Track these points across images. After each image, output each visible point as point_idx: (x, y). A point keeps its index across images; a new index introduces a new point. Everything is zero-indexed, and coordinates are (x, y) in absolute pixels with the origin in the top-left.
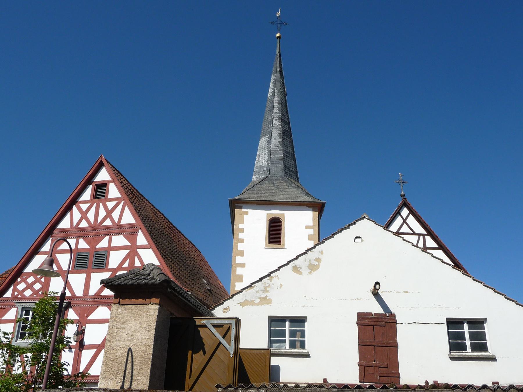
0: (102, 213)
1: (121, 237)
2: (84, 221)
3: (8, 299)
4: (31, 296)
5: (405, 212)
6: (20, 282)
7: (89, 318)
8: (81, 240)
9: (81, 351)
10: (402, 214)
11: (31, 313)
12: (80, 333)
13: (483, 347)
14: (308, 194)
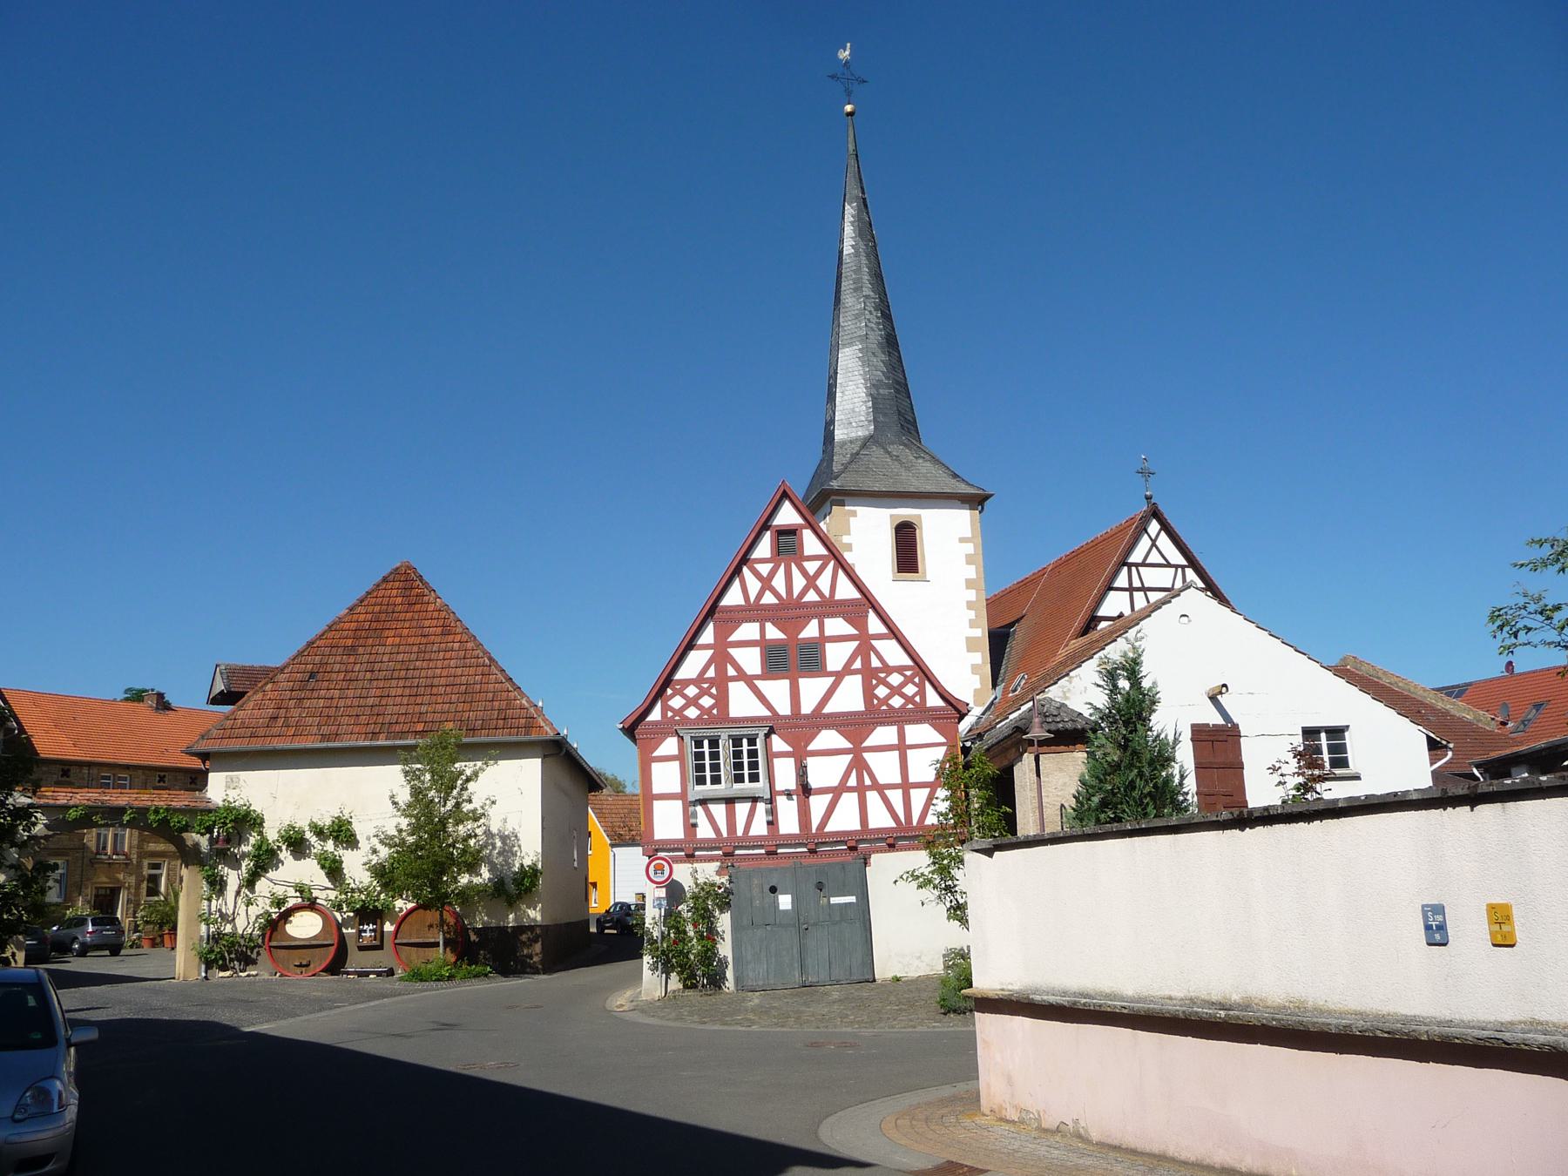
0: (799, 582)
1: (840, 620)
2: (768, 593)
3: (655, 723)
5: (1154, 527)
6: (672, 696)
8: (769, 626)
11: (706, 743)
12: (802, 772)
13: (1343, 763)
14: (955, 476)
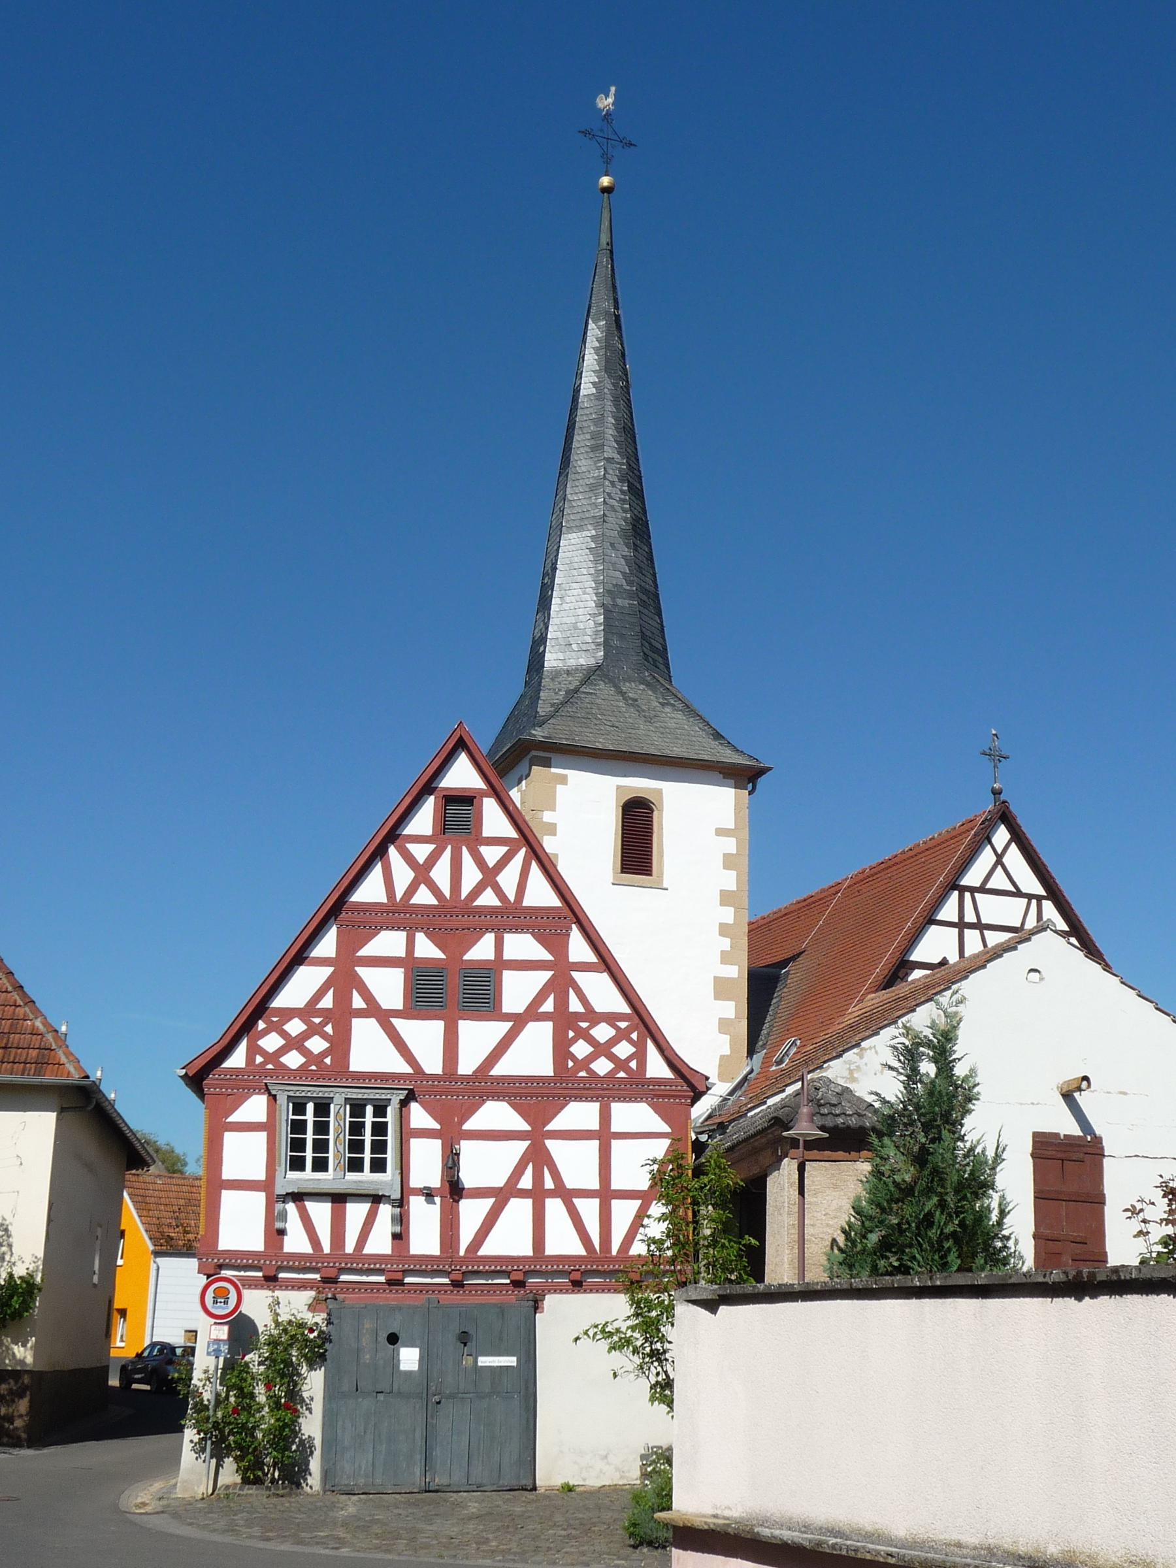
0: (471, 876)
1: (528, 938)
3: (236, 1071)
4: (303, 1068)
5: (1001, 835)
6: (265, 1032)
7: (465, 1127)
8: (420, 937)
9: (458, 1202)
10: (993, 840)
11: (310, 1107)
12: (451, 1162)
14: (717, 736)
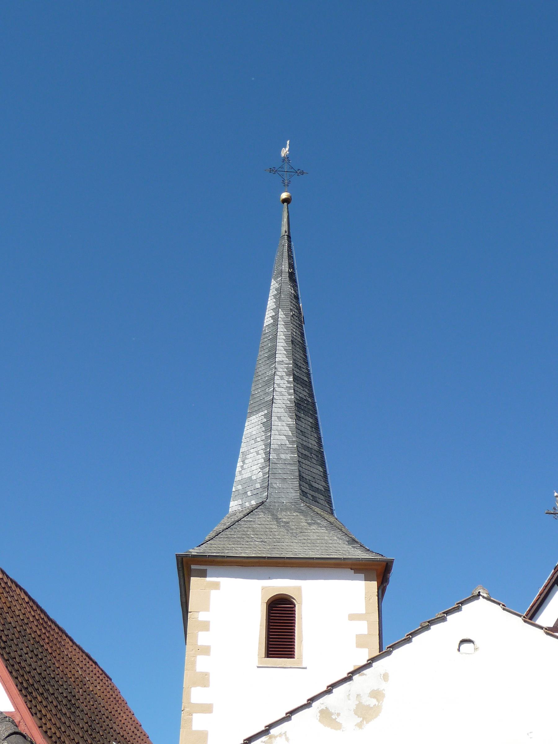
14: (353, 541)
